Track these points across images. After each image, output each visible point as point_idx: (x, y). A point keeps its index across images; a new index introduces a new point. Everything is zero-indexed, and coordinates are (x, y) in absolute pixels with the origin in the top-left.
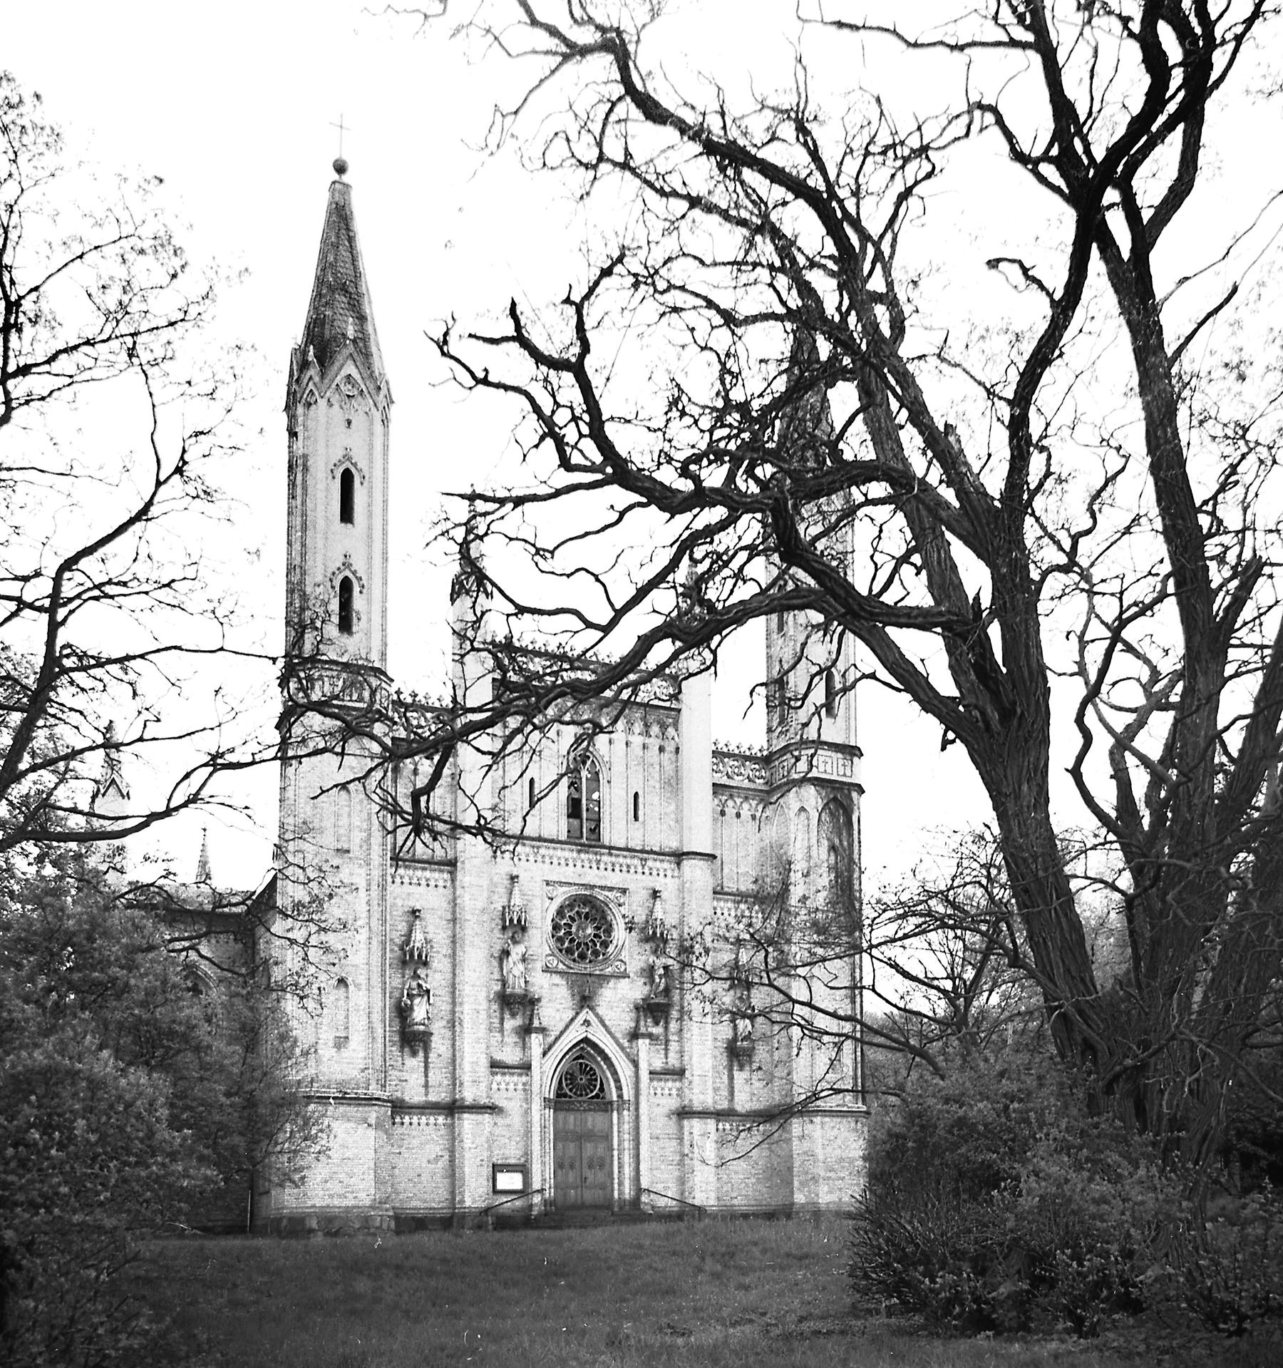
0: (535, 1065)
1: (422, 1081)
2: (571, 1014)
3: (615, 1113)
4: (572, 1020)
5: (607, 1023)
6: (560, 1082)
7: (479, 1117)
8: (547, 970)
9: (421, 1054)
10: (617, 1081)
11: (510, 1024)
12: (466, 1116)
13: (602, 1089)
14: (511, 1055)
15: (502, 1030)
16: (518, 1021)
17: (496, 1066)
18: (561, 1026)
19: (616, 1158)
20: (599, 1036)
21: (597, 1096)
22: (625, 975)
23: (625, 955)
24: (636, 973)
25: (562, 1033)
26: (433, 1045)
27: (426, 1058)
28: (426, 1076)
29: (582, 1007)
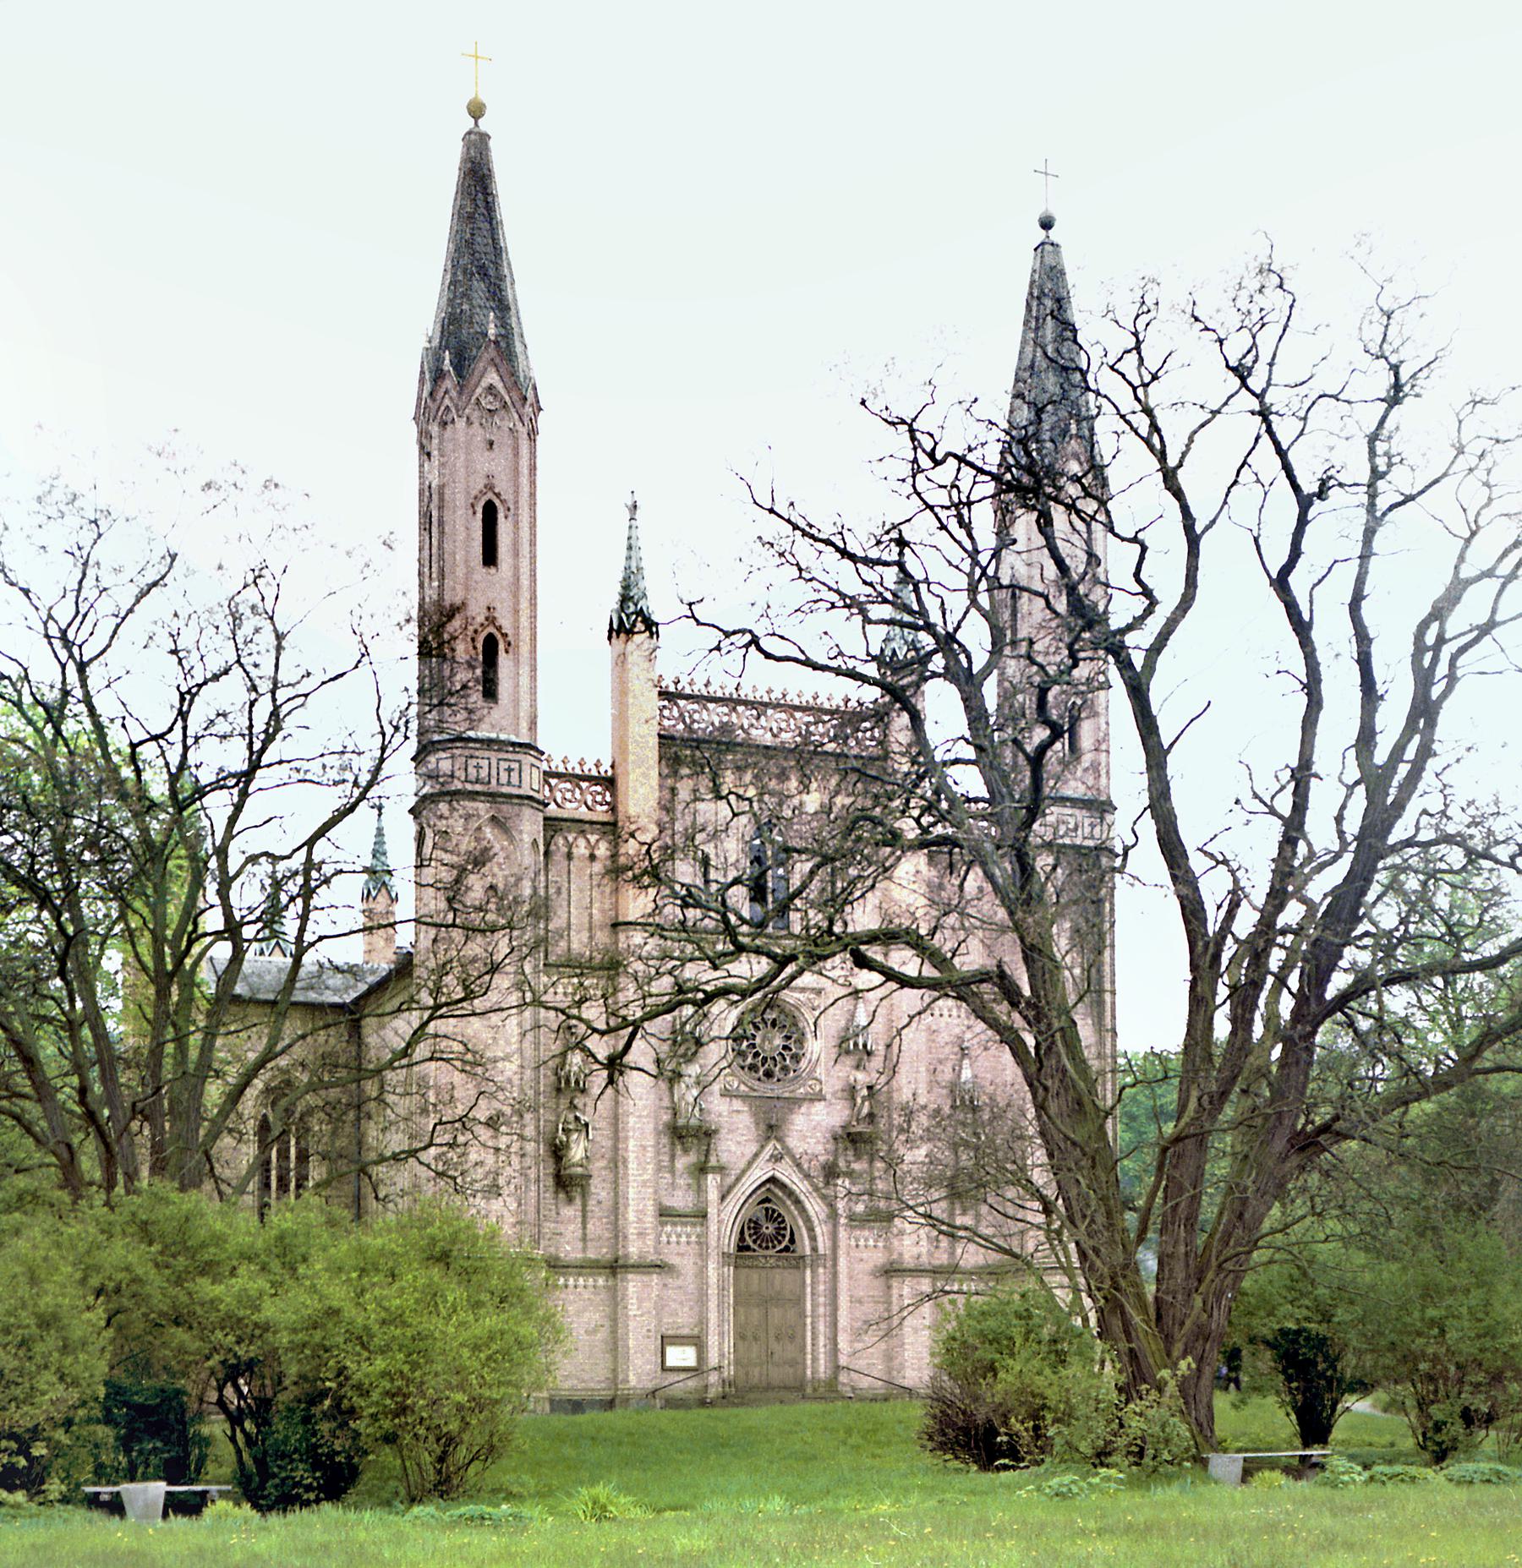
0: (712, 1211)
1: (579, 1234)
2: (754, 1148)
3: (808, 1272)
4: (756, 1155)
6: (742, 1232)
7: (645, 1278)
8: (726, 1093)
9: (578, 1201)
11: (682, 1162)
12: (630, 1276)
13: (792, 1241)
14: (681, 1200)
15: (672, 1171)
16: (692, 1158)
17: (665, 1214)
18: (742, 1164)
19: (809, 1327)
20: (786, 1173)
21: (787, 1249)
22: (820, 1097)
23: (820, 1072)
24: (834, 1094)
25: (744, 1172)
26: (593, 1189)
27: (584, 1205)
28: (584, 1228)
29: (768, 1138)
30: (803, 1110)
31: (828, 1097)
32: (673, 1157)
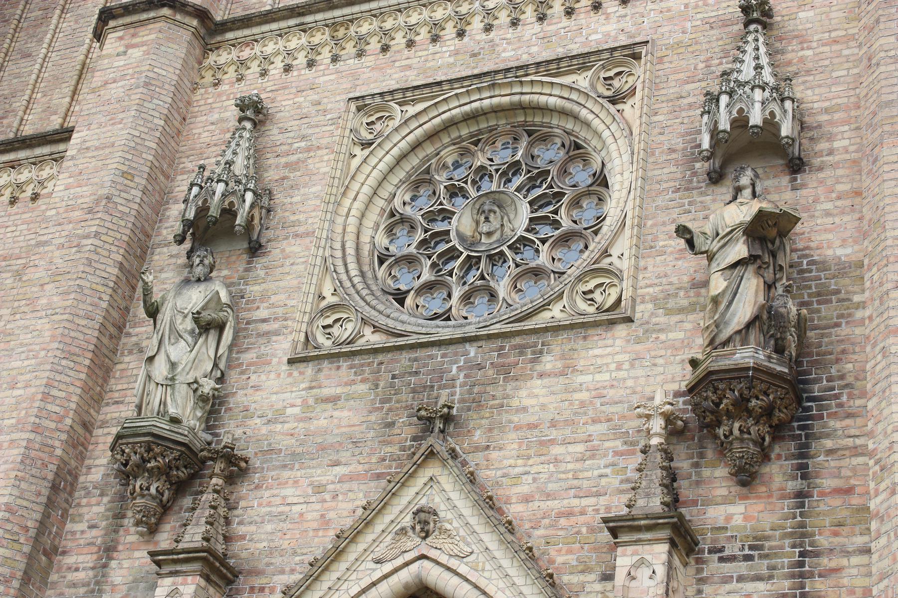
5: (514, 510)
30: (549, 362)
31: (643, 311)
32: (109, 550)
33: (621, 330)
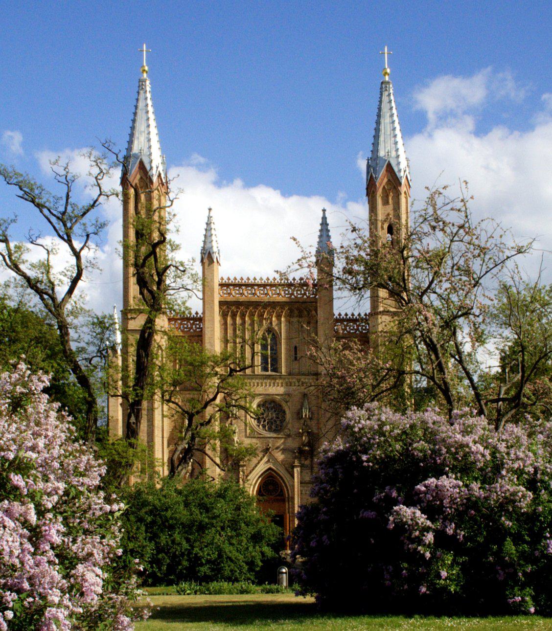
10: (287, 487)
33: (291, 439)
